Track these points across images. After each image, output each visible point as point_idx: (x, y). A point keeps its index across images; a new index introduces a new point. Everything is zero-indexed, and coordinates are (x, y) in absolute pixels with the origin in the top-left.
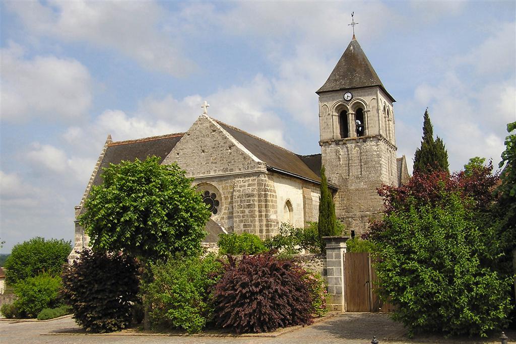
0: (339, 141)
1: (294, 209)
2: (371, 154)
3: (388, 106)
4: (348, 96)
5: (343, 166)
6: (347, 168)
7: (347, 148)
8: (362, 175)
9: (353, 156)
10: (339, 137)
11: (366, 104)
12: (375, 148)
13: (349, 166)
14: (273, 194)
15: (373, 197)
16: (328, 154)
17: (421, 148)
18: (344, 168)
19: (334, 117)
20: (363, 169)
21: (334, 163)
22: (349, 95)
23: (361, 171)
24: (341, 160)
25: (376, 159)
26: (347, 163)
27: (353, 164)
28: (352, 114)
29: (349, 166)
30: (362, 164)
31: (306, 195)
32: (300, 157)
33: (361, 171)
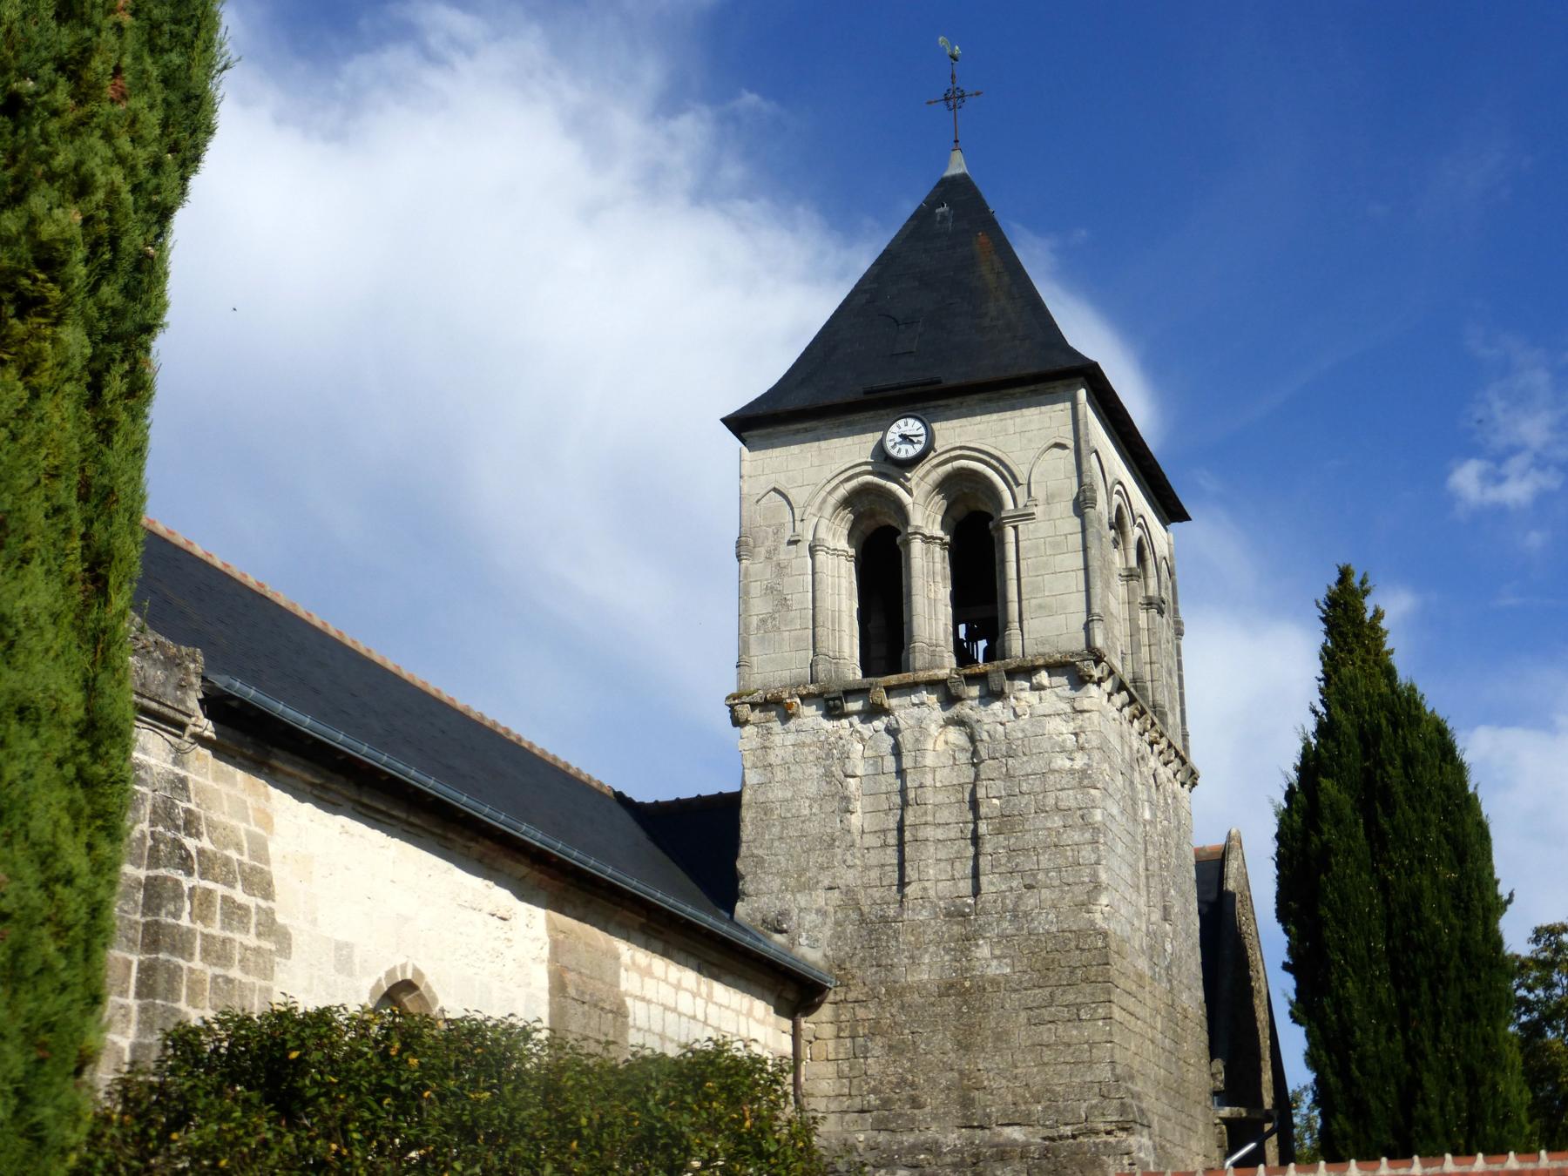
0: (851, 693)
1: (293, 954)
2: (1035, 765)
3: (1144, 527)
4: (903, 435)
5: (870, 840)
6: (891, 857)
7: (893, 732)
8: (983, 898)
9: (928, 781)
10: (853, 672)
11: (1012, 480)
12: (1061, 729)
13: (901, 844)
14: (239, 895)
15: (1046, 1034)
16: (780, 775)
17: (1323, 672)
18: (873, 858)
19: (821, 556)
20: (985, 862)
21: (813, 828)
22: (912, 426)
23: (976, 875)
24: (857, 806)
25: (1070, 799)
26: (892, 823)
27: (929, 832)
28: (928, 539)
29: (901, 844)
30: (983, 828)
31: (570, 977)
32: (620, 798)
33: (976, 875)
